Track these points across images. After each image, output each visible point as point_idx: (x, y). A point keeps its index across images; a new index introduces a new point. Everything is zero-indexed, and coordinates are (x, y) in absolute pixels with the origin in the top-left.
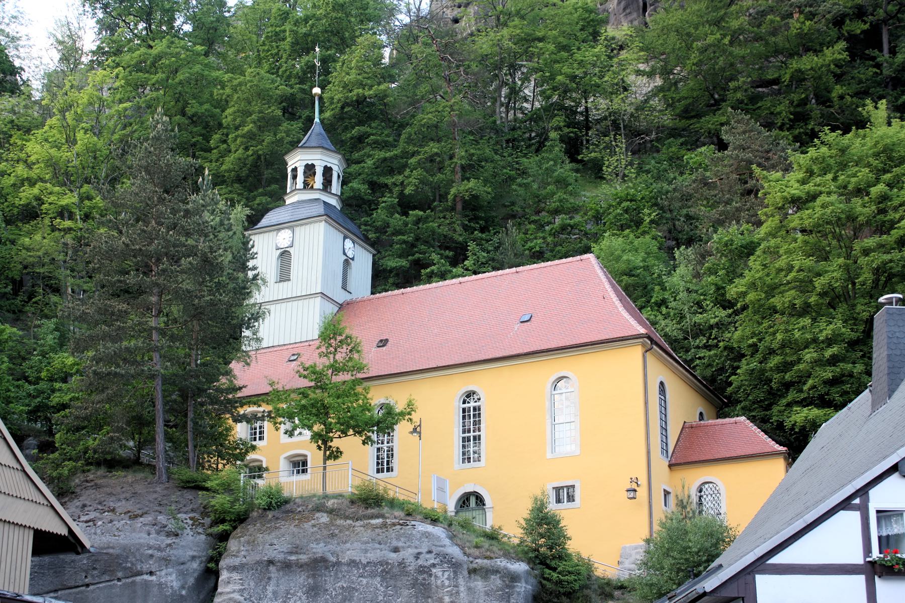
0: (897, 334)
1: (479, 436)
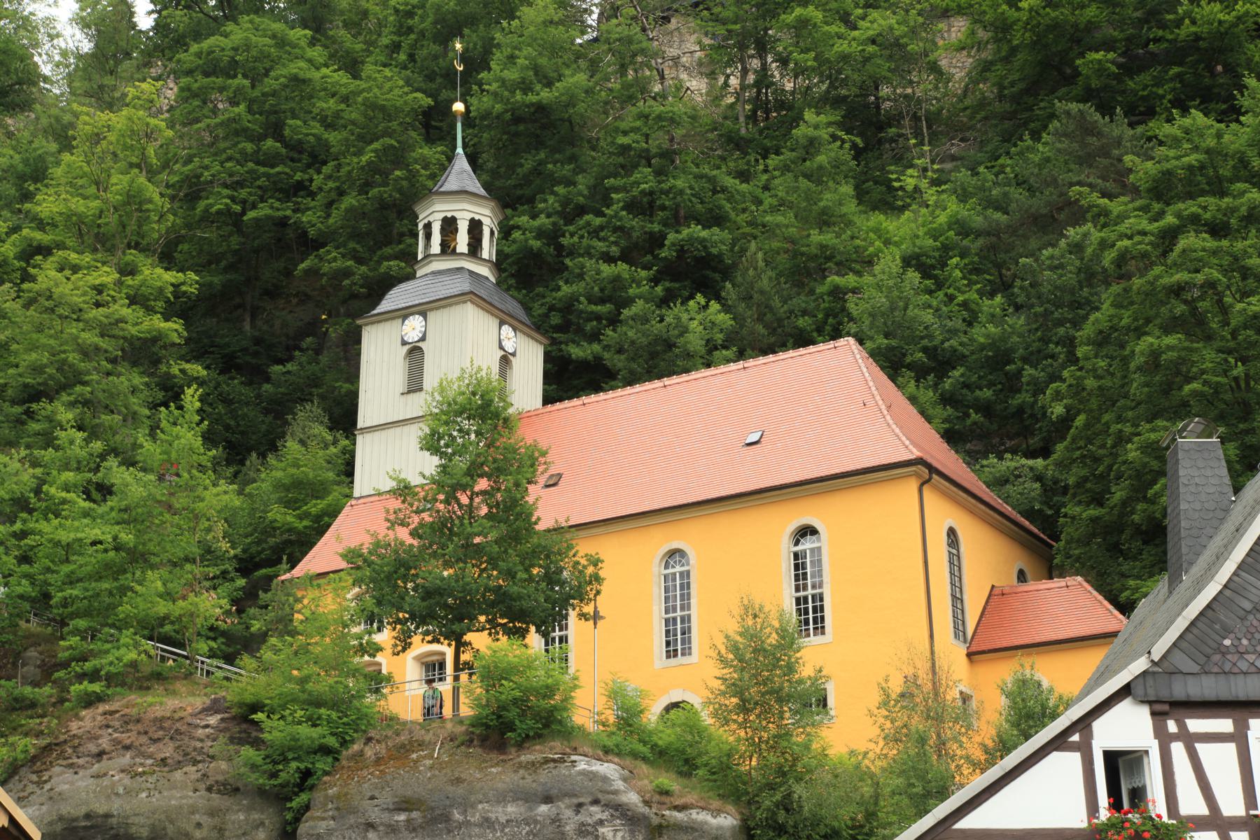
0: (1197, 480)
1: (689, 616)
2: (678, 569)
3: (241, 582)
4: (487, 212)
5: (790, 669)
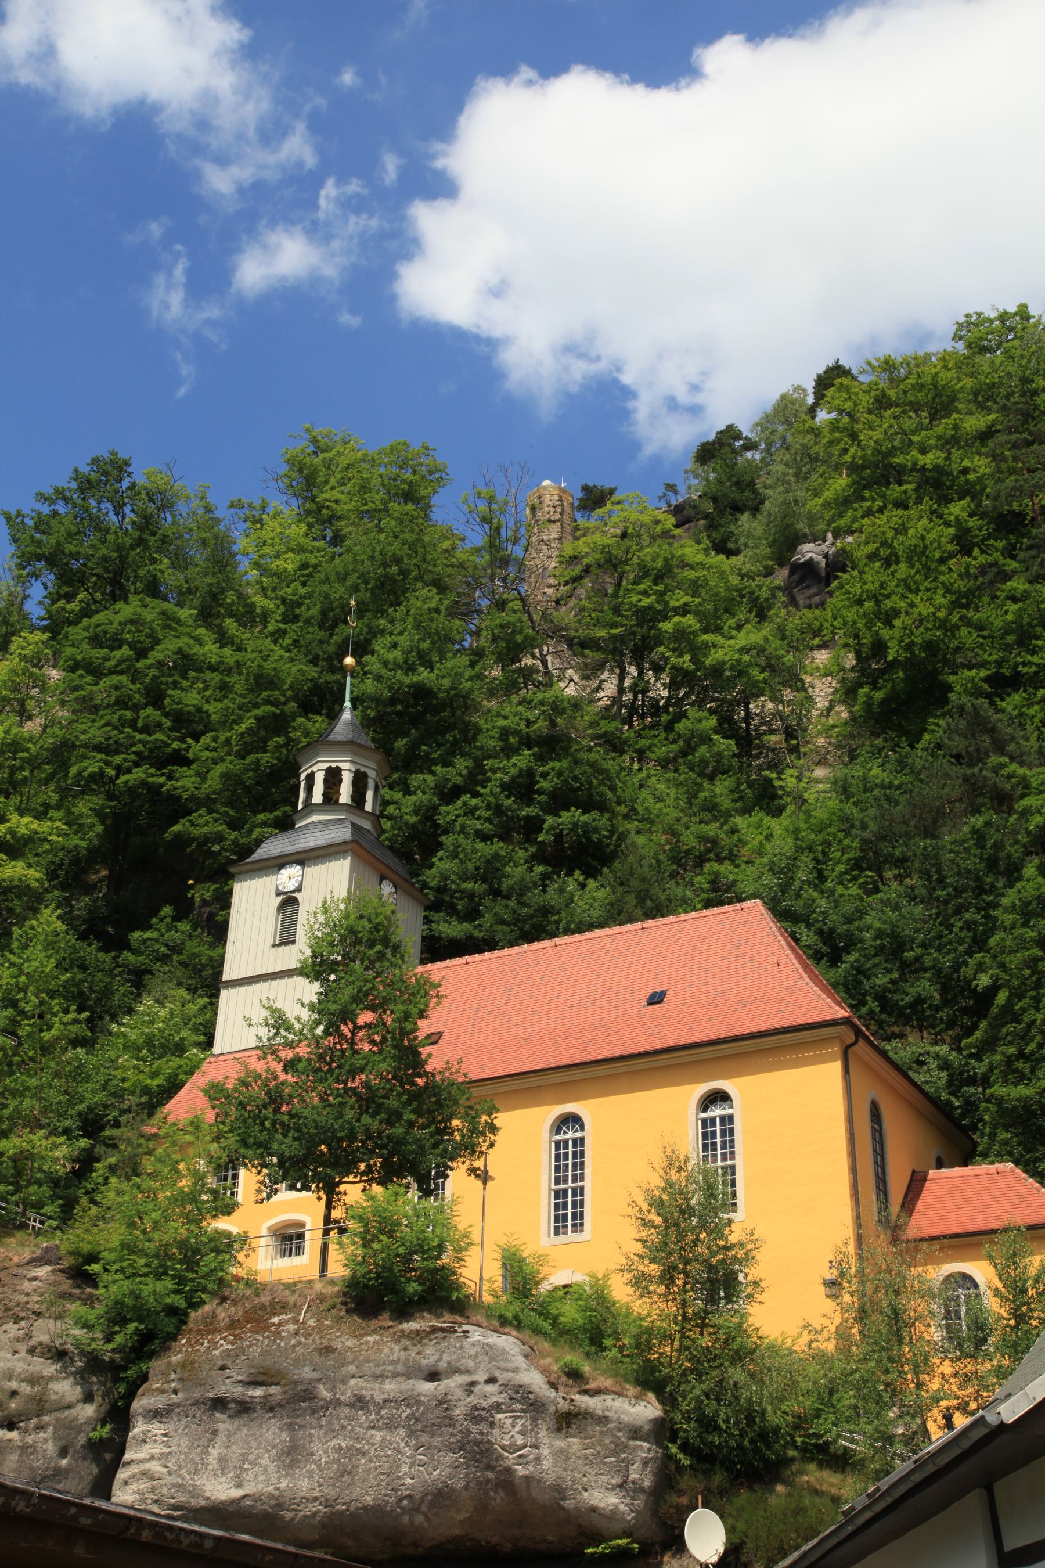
1: (582, 1188)
2: (571, 1135)
4: (374, 766)
5: (717, 1232)
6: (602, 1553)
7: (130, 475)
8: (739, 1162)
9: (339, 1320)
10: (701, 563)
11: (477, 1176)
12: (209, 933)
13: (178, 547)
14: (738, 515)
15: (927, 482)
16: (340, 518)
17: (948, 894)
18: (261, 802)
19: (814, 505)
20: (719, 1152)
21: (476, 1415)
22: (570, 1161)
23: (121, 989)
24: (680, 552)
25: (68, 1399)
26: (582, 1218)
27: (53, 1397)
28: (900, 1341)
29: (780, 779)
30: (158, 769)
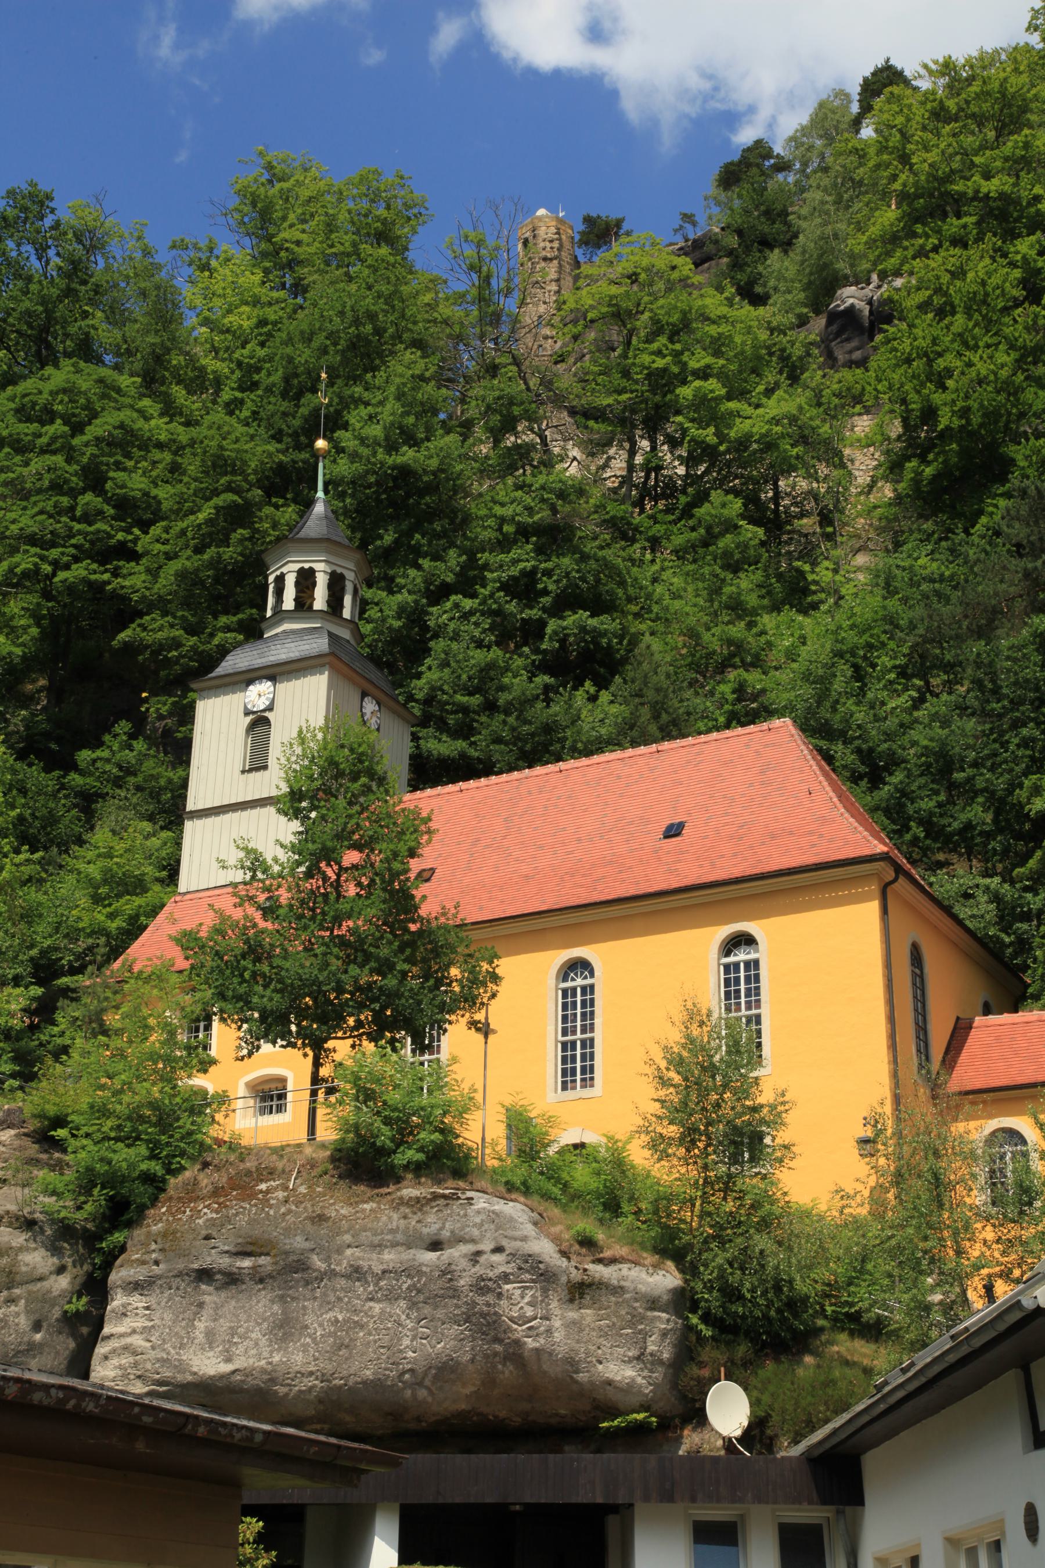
1: (592, 1040)
2: (579, 982)
3: (37, 991)
4: (351, 566)
5: (744, 1091)
6: (618, 1427)
7: (53, 211)
8: (765, 1011)
9: (331, 1187)
10: (725, 317)
11: (478, 1030)
12: (166, 753)
13: (114, 300)
14: (767, 252)
15: (990, 213)
16: (300, 263)
17: (1004, 707)
18: (222, 603)
19: (857, 243)
20: (743, 1000)
21: (481, 1286)
22: (579, 1011)
23: (69, 819)
24: (700, 303)
25: (41, 1271)
26: (592, 1071)
27: (24, 1269)
28: (941, 1206)
29: (813, 572)
30: (102, 563)
